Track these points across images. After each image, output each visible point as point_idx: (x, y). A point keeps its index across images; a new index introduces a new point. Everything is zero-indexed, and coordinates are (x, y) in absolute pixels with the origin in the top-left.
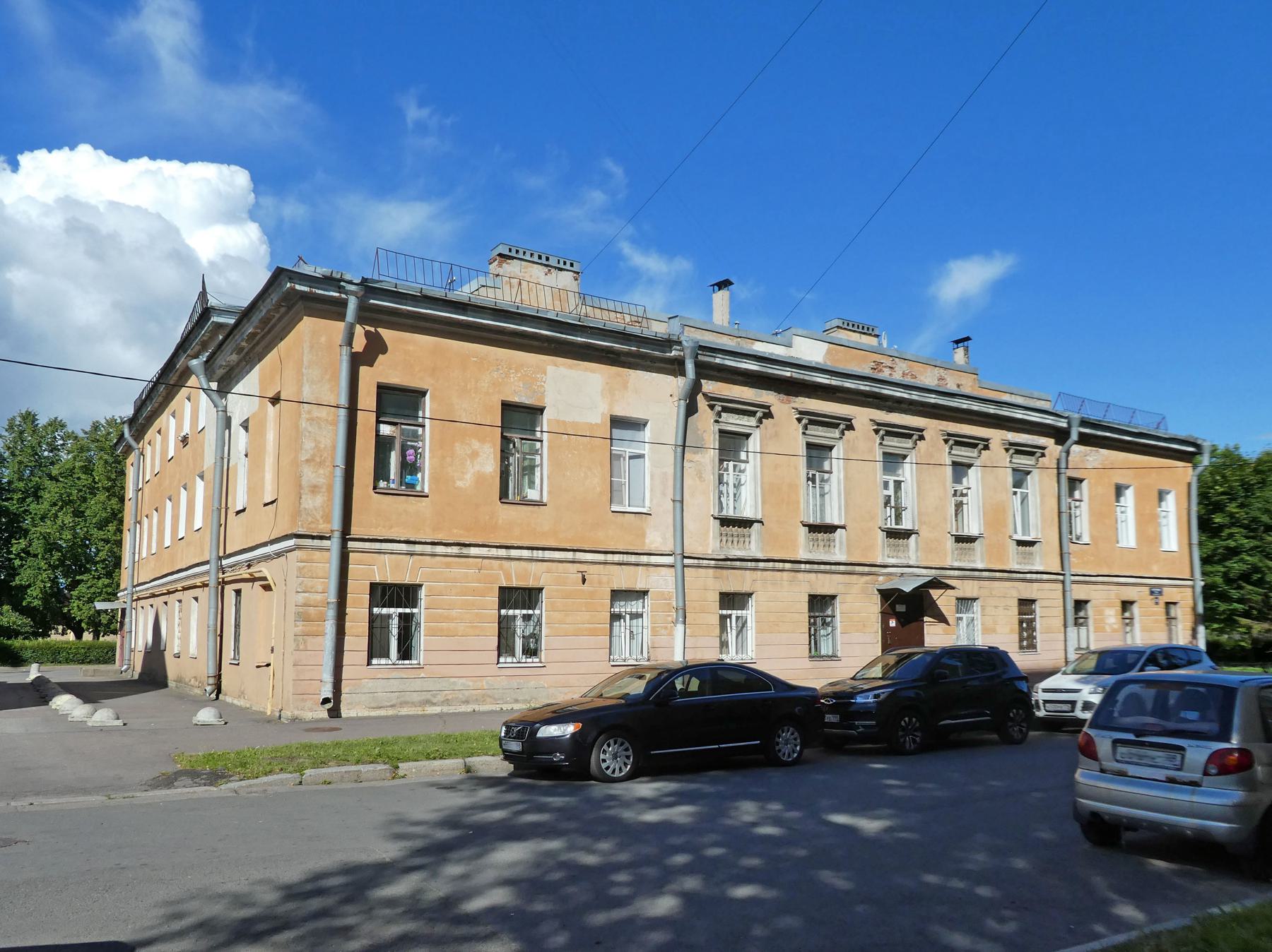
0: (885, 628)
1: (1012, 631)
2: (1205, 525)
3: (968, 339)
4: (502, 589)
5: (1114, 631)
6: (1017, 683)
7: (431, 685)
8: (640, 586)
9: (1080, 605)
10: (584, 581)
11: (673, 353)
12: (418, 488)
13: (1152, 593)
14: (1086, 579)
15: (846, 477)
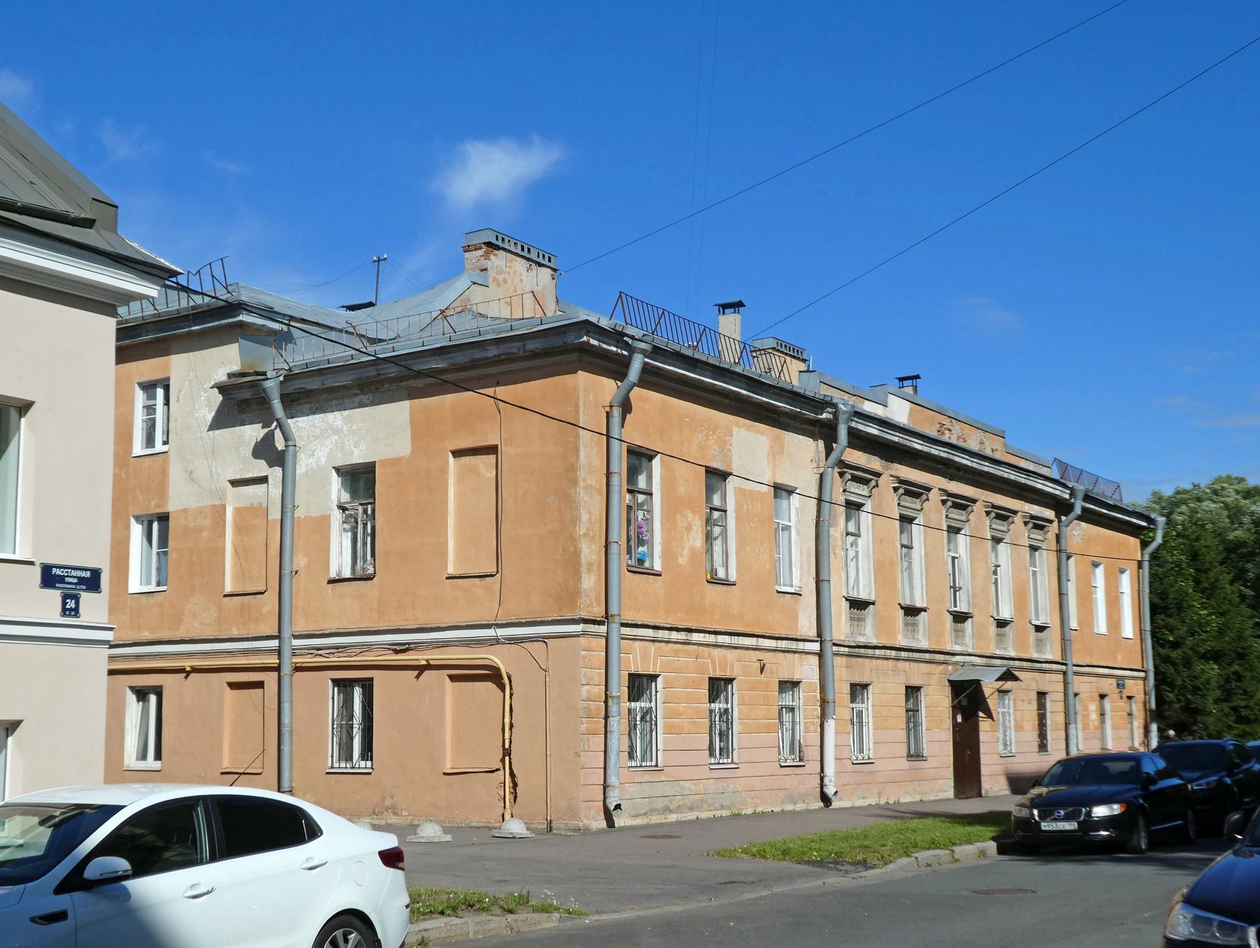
0: (955, 724)
2: (1154, 609)
3: (917, 377)
7: (668, 790)
9: (639, 685)
10: (762, 670)
11: (824, 416)
12: (647, 565)
15: (926, 554)
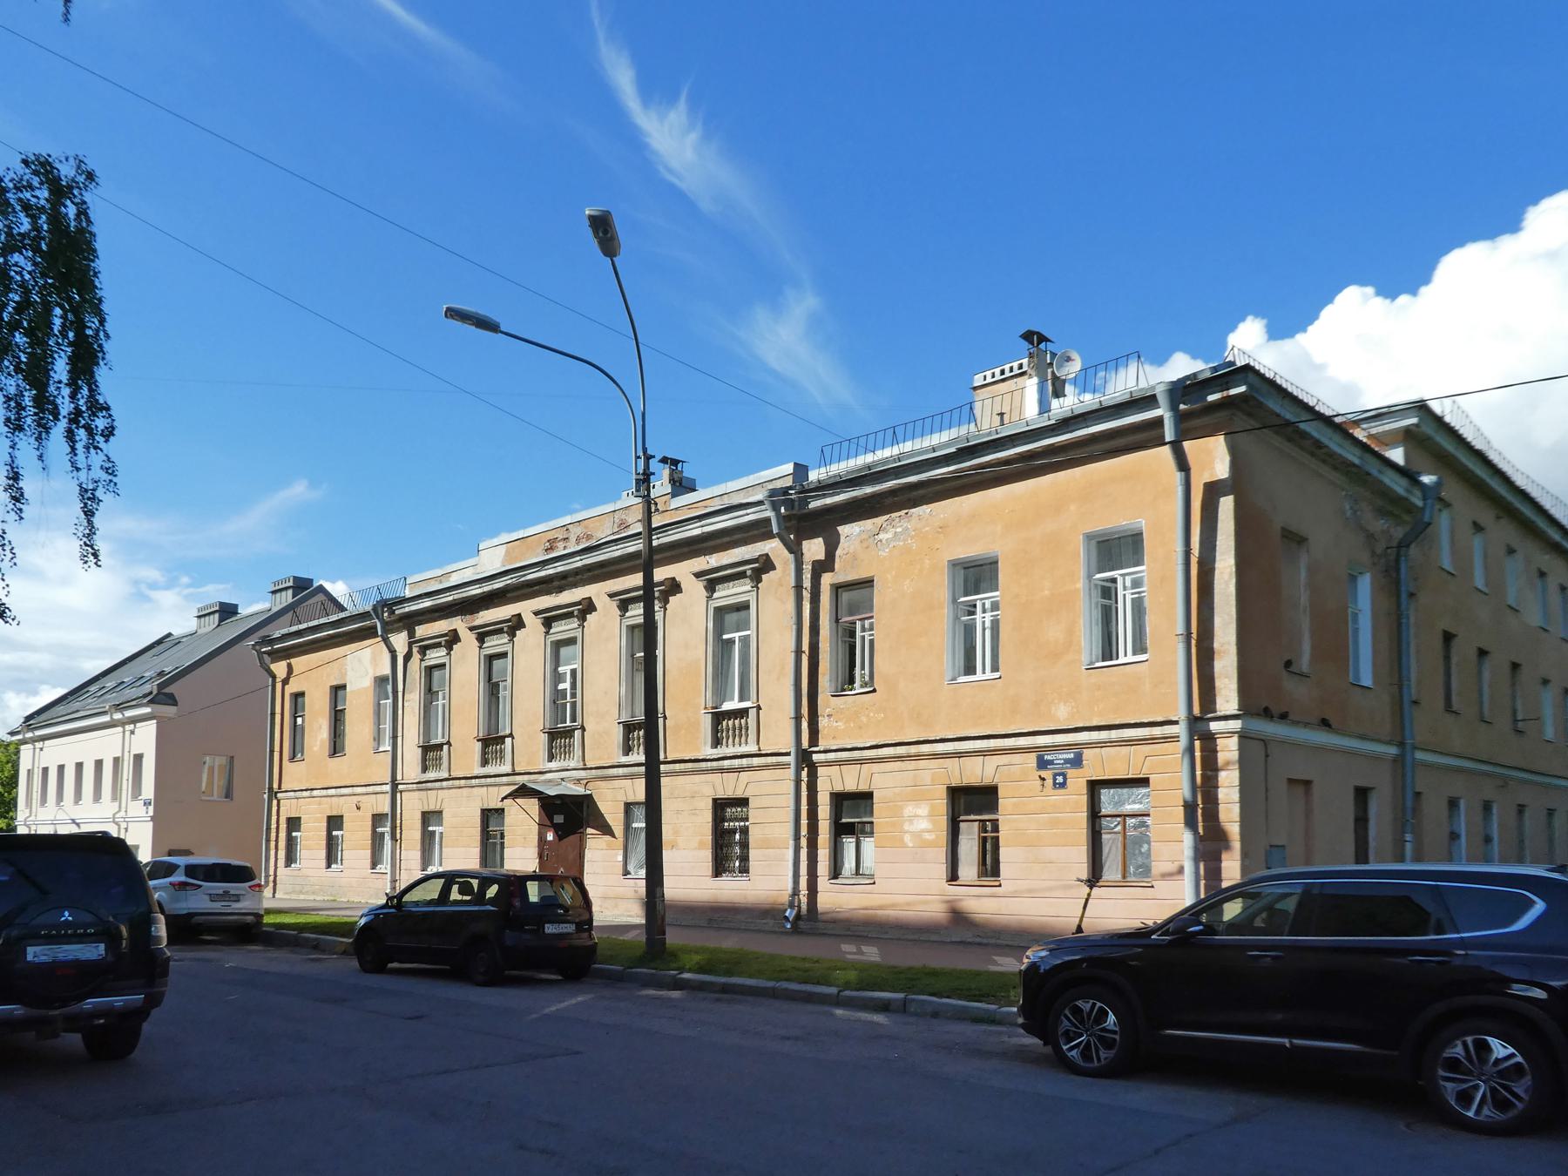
0: (542, 840)
1: (701, 846)
4: (715, 800)
5: (927, 845)
6: (406, 898)
8: (739, 794)
13: (1042, 764)
14: (856, 756)
